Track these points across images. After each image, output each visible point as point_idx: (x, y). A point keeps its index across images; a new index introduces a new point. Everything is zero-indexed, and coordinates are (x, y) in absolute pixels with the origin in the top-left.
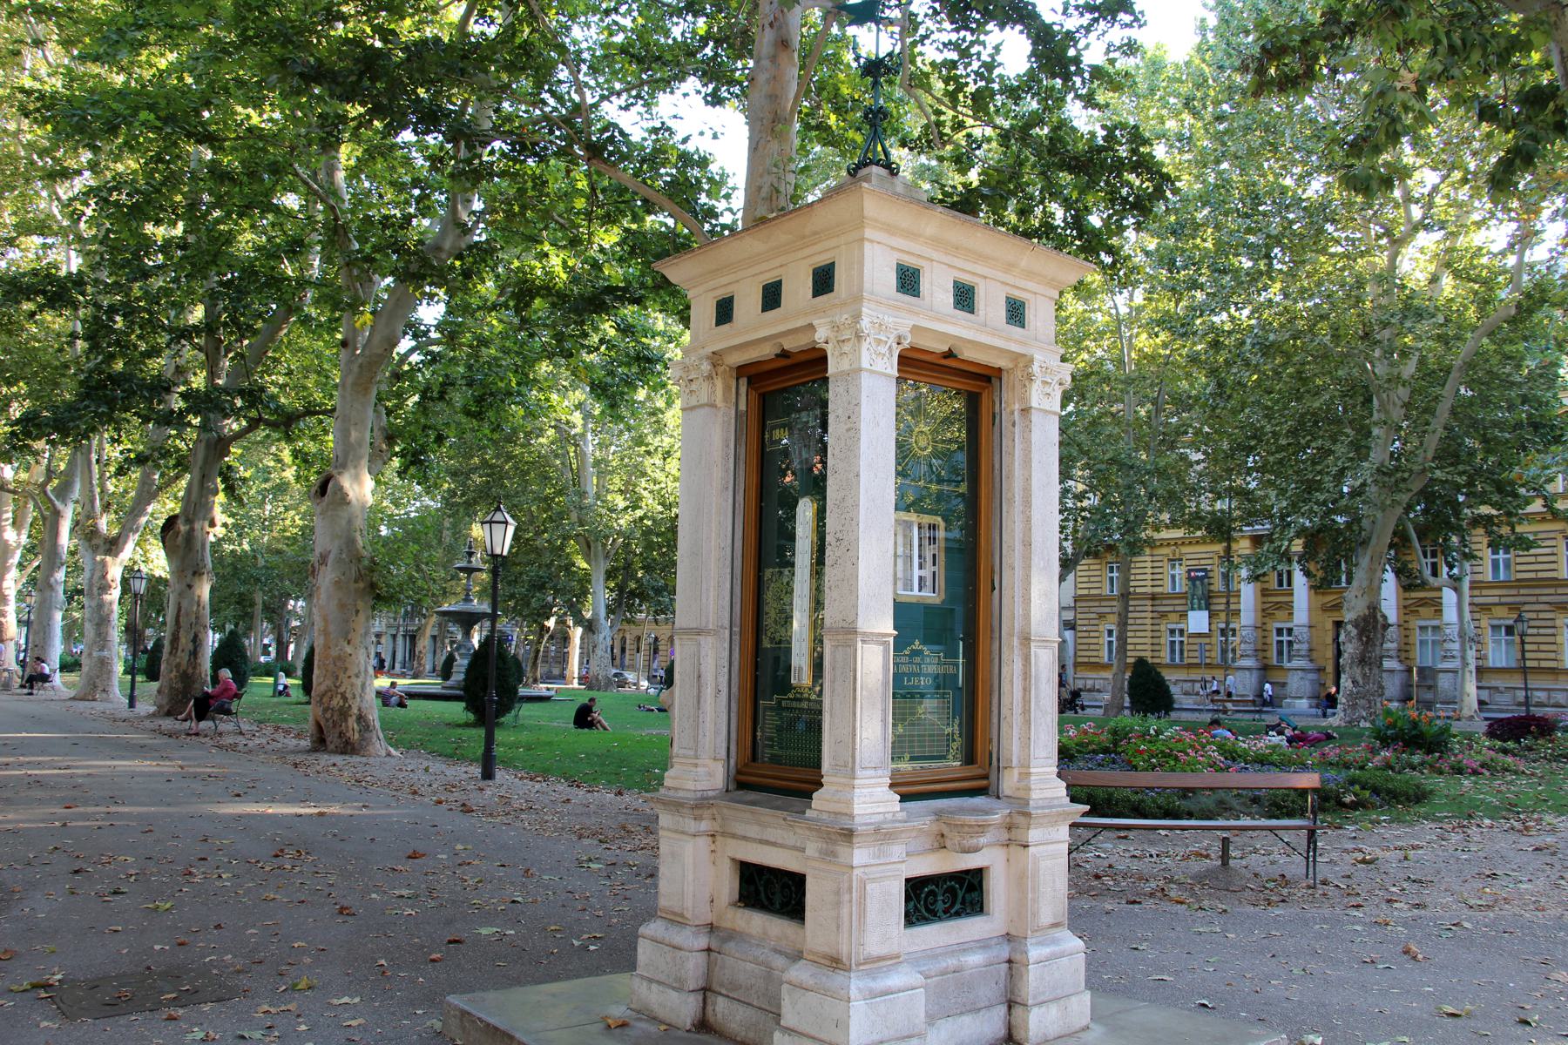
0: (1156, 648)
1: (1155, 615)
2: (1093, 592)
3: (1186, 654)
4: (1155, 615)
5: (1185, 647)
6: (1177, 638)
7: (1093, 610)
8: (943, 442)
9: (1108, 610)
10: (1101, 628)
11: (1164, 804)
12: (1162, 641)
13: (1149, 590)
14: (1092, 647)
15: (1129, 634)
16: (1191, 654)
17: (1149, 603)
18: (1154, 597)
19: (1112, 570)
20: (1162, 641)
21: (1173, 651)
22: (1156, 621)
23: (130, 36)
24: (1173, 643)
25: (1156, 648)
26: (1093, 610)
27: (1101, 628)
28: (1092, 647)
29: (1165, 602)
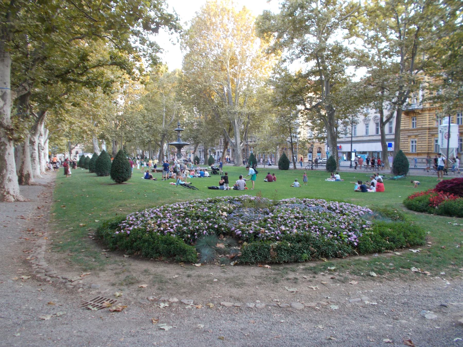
0: (430, 147)
1: (430, 135)
2: (406, 128)
3: (417, 149)
4: (430, 135)
5: (417, 147)
6: (414, 144)
7: (406, 134)
8: (347, 319)
9: (411, 134)
10: (409, 140)
11: (264, 83)
12: (432, 144)
13: (427, 126)
14: (406, 147)
15: (401, 143)
16: (419, 149)
17: (427, 131)
18: (429, 129)
19: (413, 120)
20: (432, 144)
21: (412, 148)
22: (430, 137)
23: (206, 41)
24: (412, 146)
25: (430, 147)
26: (406, 134)
27: (409, 140)
28: (406, 147)
29: (434, 130)
